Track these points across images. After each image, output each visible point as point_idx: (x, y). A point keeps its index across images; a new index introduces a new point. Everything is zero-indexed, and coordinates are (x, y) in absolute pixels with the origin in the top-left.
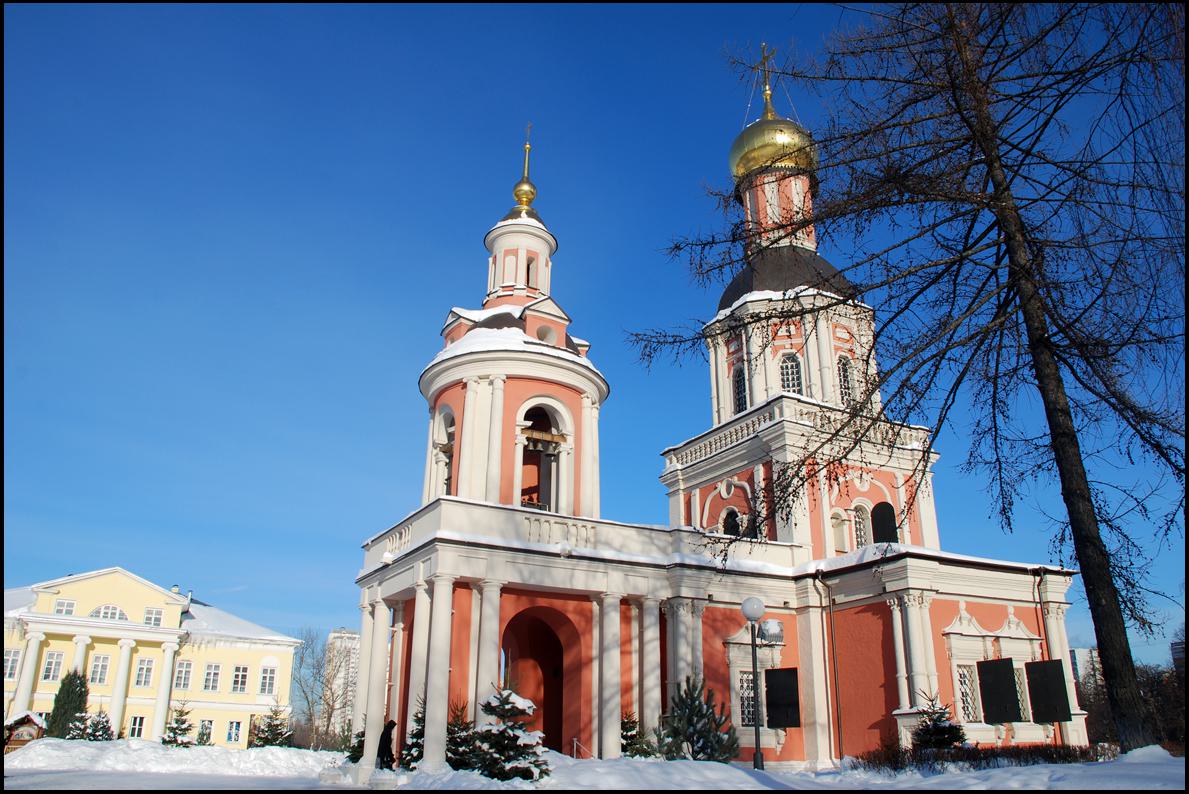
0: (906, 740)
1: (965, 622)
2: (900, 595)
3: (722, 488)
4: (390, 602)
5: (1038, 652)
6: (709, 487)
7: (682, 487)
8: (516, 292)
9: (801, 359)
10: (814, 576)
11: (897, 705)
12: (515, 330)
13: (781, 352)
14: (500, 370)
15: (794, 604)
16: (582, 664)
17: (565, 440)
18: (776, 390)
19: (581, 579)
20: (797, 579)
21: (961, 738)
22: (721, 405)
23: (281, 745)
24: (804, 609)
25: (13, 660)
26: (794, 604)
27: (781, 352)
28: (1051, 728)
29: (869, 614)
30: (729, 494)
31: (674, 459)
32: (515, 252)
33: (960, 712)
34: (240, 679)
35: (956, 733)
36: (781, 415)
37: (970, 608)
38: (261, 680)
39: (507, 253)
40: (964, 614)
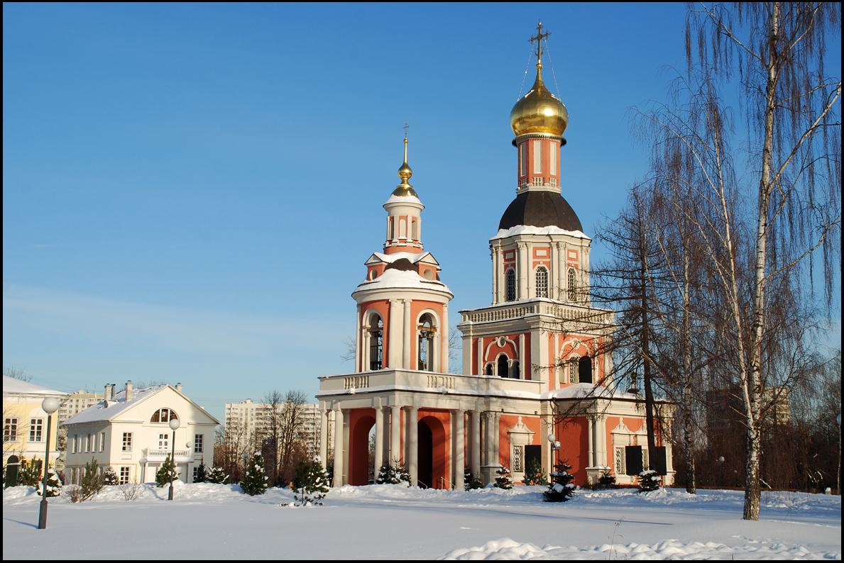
1: (622, 428)
3: (498, 340)
4: (350, 414)
6: (489, 339)
7: (472, 334)
9: (548, 271)
10: (550, 400)
11: (587, 465)
12: (413, 273)
14: (409, 297)
15: (539, 413)
16: (443, 439)
17: (436, 330)
18: (533, 297)
19: (445, 404)
20: (541, 400)
21: (615, 481)
22: (499, 290)
23: (225, 483)
24: (544, 416)
25: (38, 427)
26: (539, 413)
30: (502, 345)
32: (406, 218)
33: (616, 469)
34: (36, 430)
35: (613, 480)
37: (625, 421)
38: (29, 429)
39: (401, 217)
40: (622, 423)
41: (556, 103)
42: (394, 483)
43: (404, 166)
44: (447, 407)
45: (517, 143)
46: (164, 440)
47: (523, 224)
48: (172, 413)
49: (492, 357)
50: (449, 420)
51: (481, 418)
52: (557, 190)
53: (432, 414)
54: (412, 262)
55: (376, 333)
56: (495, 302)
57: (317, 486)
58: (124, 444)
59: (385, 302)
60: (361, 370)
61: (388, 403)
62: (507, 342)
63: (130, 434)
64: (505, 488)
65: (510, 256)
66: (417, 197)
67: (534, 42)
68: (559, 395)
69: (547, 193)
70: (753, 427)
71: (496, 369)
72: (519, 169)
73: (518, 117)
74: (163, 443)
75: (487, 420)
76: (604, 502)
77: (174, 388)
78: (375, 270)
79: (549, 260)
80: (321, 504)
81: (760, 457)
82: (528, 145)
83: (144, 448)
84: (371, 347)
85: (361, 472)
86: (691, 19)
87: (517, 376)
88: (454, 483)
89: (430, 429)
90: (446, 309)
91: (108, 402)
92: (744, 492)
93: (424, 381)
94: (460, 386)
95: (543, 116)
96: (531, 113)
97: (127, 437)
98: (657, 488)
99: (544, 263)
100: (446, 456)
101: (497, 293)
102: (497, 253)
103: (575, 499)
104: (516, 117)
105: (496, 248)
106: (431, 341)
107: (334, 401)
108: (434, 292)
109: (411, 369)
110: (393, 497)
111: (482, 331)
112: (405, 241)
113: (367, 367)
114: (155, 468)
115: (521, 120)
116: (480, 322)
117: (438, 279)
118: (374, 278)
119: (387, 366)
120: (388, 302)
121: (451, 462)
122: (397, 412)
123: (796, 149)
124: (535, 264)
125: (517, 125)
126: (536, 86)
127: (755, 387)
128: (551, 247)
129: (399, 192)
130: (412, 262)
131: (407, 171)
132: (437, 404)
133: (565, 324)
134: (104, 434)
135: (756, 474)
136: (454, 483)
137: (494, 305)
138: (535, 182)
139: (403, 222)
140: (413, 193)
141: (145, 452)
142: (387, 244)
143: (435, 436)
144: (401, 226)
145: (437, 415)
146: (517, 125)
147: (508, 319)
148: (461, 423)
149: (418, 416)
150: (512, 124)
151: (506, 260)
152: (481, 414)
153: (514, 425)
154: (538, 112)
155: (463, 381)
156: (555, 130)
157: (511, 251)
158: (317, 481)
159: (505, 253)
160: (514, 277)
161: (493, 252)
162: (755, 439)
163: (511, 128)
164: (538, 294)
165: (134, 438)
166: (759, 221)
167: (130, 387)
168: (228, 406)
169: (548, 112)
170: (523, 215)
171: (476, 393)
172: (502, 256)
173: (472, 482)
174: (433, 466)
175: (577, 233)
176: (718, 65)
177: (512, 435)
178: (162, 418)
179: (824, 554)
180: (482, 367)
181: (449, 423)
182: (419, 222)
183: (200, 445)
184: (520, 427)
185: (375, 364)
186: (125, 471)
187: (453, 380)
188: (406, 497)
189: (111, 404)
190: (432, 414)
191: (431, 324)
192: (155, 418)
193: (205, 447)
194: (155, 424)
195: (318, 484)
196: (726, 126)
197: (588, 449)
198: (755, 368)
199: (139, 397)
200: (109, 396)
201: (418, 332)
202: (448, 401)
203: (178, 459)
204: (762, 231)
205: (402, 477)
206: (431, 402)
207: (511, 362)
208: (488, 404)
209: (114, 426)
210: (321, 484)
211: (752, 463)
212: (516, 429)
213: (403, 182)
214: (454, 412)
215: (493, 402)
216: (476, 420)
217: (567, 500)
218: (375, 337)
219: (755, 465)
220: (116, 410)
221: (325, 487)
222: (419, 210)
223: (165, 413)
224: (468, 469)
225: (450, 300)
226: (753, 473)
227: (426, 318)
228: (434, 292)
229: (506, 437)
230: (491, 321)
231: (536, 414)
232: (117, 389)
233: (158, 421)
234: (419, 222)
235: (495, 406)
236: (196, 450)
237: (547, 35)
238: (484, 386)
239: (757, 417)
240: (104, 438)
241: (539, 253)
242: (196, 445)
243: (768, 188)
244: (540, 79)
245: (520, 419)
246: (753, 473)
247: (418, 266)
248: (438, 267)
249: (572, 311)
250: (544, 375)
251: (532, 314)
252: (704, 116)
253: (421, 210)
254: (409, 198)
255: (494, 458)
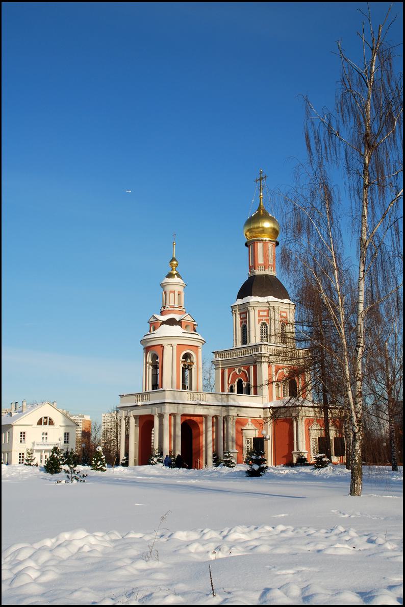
0: (295, 461)
2: (296, 418)
3: (237, 370)
4: (139, 418)
5: (323, 434)
6: (231, 369)
7: (220, 367)
8: (175, 309)
9: (268, 325)
10: (269, 408)
12: (178, 327)
13: (261, 322)
14: (175, 343)
15: (262, 417)
16: (199, 434)
17: (194, 364)
18: (258, 341)
19: (200, 411)
20: (264, 408)
22: (237, 338)
24: (265, 418)
26: (262, 417)
27: (261, 322)
28: (339, 458)
29: (285, 423)
31: (218, 355)
32: (174, 292)
36: (261, 351)
39: (171, 292)
41: (272, 219)
42: (152, 464)
43: (173, 259)
44: (201, 414)
45: (248, 245)
46: (45, 436)
47: (251, 296)
48: (50, 419)
49: (233, 381)
50: (203, 422)
51: (223, 421)
52: (273, 274)
53: (192, 418)
54: (178, 320)
55: (155, 367)
56: (234, 346)
57: (98, 467)
58: (21, 439)
59: (160, 346)
60: (146, 390)
61: (161, 411)
62: (242, 371)
63: (24, 433)
64: (230, 467)
65: (243, 316)
66: (181, 278)
67: (258, 182)
68: (275, 404)
69: (267, 276)
70: (356, 424)
71: (235, 388)
72: (249, 261)
73: (247, 229)
74: (45, 438)
75: (227, 421)
76: (286, 478)
77: (52, 404)
78: (154, 325)
79: (268, 318)
80: (84, 481)
81: (362, 446)
82: (254, 246)
83: (33, 441)
84: (152, 375)
85: (145, 457)
86: (309, 125)
87: (249, 393)
88: (206, 463)
89: (190, 428)
90: (200, 350)
91: (12, 413)
92: (350, 470)
93: (185, 397)
94: (209, 399)
95: (263, 228)
96: (256, 226)
97: (23, 435)
98: (326, 466)
99: (266, 320)
100: (201, 445)
101: (236, 340)
102: (235, 314)
103: (267, 475)
104: (247, 228)
105: (235, 311)
106: (191, 370)
107: (129, 410)
108: (191, 339)
109: (177, 389)
110: (149, 474)
111: (228, 364)
112: (173, 307)
113: (150, 388)
114: (40, 453)
115: (250, 230)
116: (226, 359)
117: (195, 330)
118: (154, 331)
119: (162, 387)
120: (162, 346)
121: (204, 449)
122: (166, 417)
123: (385, 214)
124: (259, 320)
125: (248, 234)
126: (259, 210)
127: (357, 393)
128: (269, 310)
129: (170, 276)
130: (178, 320)
131: (175, 262)
132: (194, 411)
133: (270, 357)
134: (9, 432)
135: (359, 459)
136: (206, 463)
137: (234, 348)
138: (259, 269)
139: (172, 294)
140: (179, 276)
141: (33, 444)
142: (163, 309)
143: (194, 432)
144: (171, 297)
145: (195, 419)
146: (248, 234)
147: (243, 356)
148: (210, 424)
149: (181, 419)
150: (245, 233)
151: (241, 319)
152: (224, 417)
153: (246, 424)
154: (260, 225)
155: (212, 396)
156: (272, 236)
157: (244, 312)
158: (98, 464)
159: (240, 314)
160: (246, 329)
161: (233, 314)
162: (357, 432)
163: (244, 235)
164: (262, 340)
165: (26, 435)
166: (360, 268)
167: (25, 404)
168: (103, 415)
169: (267, 225)
170: (251, 290)
171: (221, 404)
172: (239, 316)
173: (217, 462)
174: (193, 452)
175: (286, 301)
176: (329, 156)
177: (244, 431)
178: (44, 422)
179: (366, 538)
180: (227, 387)
181: (203, 424)
182: (183, 295)
183: (68, 439)
184: (250, 426)
185: (155, 386)
186: (22, 456)
187: (204, 396)
188: (159, 474)
189: (14, 414)
190: (192, 418)
191: (191, 360)
192: (40, 423)
193: (70, 440)
194: (40, 426)
195: (98, 466)
196: (335, 200)
197: (293, 440)
198: (358, 378)
199: (30, 409)
200: (14, 409)
201: (182, 365)
202: (202, 409)
203: (59, 448)
204: (362, 276)
205: (158, 461)
206: (190, 410)
207: (245, 384)
208: (228, 411)
209: (15, 428)
210: (101, 466)
211: (356, 451)
212: (247, 427)
213: (172, 270)
214: (206, 416)
215: (231, 410)
216: (220, 422)
217: (261, 475)
218: (155, 368)
219: (358, 452)
220: (17, 417)
221: (104, 468)
222: (183, 287)
223: (45, 419)
224: (215, 454)
225: (203, 344)
226: (357, 458)
227: (187, 356)
228: (191, 339)
229: (240, 432)
230: (232, 358)
231: (260, 417)
232: (19, 405)
233: (41, 424)
234: (183, 295)
235: (233, 412)
236: (65, 442)
237: (265, 177)
238: (225, 399)
239: (359, 416)
240: (9, 435)
241: (262, 313)
242: (65, 439)
243: (365, 243)
244: (262, 204)
245: (250, 420)
246: (357, 458)
247: (181, 322)
248: (195, 323)
249: (270, 349)
250: (265, 390)
251: (258, 353)
252: (321, 192)
253: (184, 287)
254: (176, 279)
255: (233, 446)
